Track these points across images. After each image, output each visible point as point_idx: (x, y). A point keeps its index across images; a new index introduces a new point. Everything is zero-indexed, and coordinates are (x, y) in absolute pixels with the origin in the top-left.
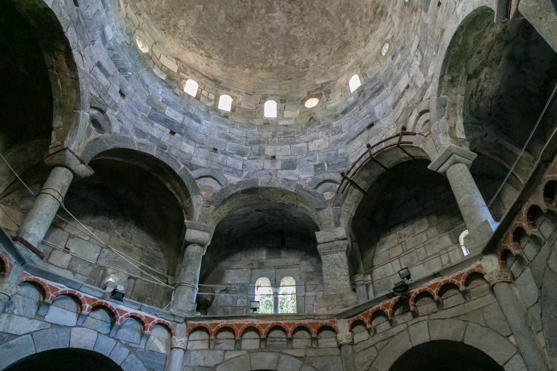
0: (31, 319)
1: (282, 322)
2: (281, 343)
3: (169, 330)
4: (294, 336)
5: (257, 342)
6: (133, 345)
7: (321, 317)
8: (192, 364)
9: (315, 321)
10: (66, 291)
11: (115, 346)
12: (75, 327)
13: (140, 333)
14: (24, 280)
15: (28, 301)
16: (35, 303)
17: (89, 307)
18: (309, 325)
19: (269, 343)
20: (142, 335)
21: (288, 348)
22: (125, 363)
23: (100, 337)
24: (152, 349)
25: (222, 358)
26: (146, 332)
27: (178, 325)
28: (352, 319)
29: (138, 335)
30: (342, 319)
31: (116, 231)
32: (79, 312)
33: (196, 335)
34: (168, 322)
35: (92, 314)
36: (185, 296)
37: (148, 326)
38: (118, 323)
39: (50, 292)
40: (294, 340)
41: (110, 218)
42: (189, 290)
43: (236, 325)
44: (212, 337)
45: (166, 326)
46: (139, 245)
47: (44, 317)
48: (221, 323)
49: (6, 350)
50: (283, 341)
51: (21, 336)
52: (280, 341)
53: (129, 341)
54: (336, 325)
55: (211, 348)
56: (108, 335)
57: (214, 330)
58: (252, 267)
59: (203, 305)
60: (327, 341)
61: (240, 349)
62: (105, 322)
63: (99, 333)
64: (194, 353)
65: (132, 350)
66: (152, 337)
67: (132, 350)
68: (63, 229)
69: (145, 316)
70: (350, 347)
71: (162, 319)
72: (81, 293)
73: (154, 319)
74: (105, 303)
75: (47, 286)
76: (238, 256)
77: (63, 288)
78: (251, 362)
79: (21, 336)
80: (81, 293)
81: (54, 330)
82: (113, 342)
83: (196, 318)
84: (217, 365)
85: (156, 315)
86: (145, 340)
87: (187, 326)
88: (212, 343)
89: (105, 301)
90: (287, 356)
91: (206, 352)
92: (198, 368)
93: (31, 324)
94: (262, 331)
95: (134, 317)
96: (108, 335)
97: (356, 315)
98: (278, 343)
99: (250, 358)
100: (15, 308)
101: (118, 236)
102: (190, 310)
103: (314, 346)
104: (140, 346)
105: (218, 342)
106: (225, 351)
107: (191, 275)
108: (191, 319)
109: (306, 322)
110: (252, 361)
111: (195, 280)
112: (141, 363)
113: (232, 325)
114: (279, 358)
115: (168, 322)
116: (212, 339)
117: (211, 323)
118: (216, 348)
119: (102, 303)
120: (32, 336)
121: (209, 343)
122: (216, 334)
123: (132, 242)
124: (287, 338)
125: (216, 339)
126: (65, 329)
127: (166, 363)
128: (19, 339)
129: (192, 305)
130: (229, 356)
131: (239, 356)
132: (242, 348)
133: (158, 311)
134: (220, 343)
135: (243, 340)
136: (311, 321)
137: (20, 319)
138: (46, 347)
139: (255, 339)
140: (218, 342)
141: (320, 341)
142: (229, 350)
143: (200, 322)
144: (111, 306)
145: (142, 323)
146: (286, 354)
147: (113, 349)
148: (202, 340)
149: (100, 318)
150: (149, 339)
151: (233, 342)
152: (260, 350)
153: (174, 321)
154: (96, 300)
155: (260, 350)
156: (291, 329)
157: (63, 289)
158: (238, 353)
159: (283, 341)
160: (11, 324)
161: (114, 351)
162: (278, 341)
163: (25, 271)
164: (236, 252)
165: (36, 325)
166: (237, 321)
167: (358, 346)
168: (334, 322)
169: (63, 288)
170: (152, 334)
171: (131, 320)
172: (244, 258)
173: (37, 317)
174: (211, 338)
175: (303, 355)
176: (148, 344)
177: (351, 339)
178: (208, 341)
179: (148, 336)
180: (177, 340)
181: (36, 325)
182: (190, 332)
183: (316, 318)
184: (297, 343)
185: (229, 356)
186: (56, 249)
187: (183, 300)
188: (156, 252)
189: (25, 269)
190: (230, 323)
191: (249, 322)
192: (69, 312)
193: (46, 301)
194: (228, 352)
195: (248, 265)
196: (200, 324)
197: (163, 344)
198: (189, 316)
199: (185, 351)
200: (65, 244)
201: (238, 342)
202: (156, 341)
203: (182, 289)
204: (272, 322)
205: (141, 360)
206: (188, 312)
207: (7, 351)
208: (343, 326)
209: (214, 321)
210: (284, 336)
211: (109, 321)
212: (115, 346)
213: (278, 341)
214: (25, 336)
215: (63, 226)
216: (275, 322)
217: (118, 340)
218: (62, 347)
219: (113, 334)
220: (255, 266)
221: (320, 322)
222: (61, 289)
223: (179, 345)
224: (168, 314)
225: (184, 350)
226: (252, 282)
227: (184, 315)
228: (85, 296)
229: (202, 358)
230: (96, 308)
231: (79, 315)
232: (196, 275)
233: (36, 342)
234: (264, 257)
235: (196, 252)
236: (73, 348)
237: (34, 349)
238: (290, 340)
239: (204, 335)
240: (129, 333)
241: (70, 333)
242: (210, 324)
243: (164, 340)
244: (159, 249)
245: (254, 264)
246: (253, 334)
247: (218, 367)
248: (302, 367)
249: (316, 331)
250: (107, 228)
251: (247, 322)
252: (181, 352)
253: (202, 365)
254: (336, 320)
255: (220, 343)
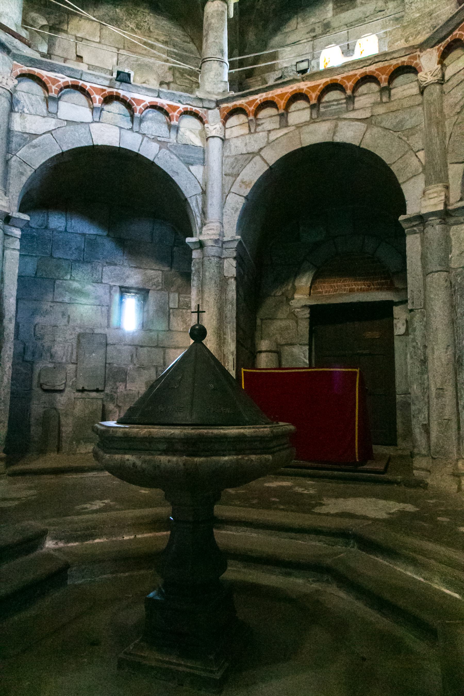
0: (44, 117)
1: (339, 77)
2: (339, 106)
3: (200, 119)
4: (356, 94)
5: (308, 112)
6: (163, 139)
7: (395, 55)
8: (234, 153)
9: (386, 64)
10: (68, 82)
11: (142, 141)
12: (92, 122)
13: (166, 125)
14: (19, 73)
15: (33, 98)
16: (41, 99)
17: (99, 99)
18: (377, 72)
19: (322, 110)
20: (170, 127)
21: (347, 111)
22: (158, 158)
23: (123, 132)
24: (184, 142)
25: (266, 140)
26: (172, 123)
27: (210, 111)
28: (443, 43)
29: (165, 128)
30: (428, 50)
31: (128, 23)
32: (92, 107)
33: (234, 120)
34: (197, 109)
35: (107, 107)
36: (212, 74)
37: (173, 116)
38: (137, 114)
39: (51, 85)
40: (356, 99)
41: (116, 6)
42: (215, 65)
43: (278, 96)
44: (251, 117)
45: (195, 115)
46: (162, 38)
47: (56, 114)
48: (260, 98)
49: (32, 150)
50: (342, 104)
51: (41, 135)
52: (338, 104)
53: (157, 135)
54: (418, 61)
55: (252, 131)
56: (131, 129)
57: (252, 108)
58: (313, 34)
59: (239, 83)
60: (405, 88)
61: (287, 126)
62: (124, 115)
63: (121, 128)
64: (235, 141)
65: (163, 144)
66: (182, 130)
67: (163, 144)
68: (66, 32)
69: (168, 105)
70: (438, 87)
71: (189, 107)
72: (86, 83)
73: (179, 107)
74: (116, 92)
75: (46, 78)
76: (293, 23)
77: (63, 78)
78: (300, 138)
79: (41, 135)
80: (86, 83)
81: (72, 128)
82: (139, 137)
83: (228, 98)
84: (261, 149)
85: (180, 102)
86: (175, 133)
87: (220, 111)
88: (254, 125)
89: (115, 90)
90: (346, 122)
91: (247, 137)
92: (241, 156)
93: (45, 122)
94: (311, 96)
95: (154, 107)
96: (131, 129)
97: (451, 32)
98: (334, 107)
99: (299, 133)
100: (23, 107)
101: (132, 29)
102: (221, 91)
103: (385, 99)
104: (171, 140)
105: (260, 122)
106: (269, 131)
107: (215, 44)
108: (223, 101)
109: (373, 68)
110: (302, 136)
111: (222, 52)
112: (175, 157)
113: (273, 97)
114: (336, 126)
115: (197, 109)
116: (251, 120)
117: (247, 100)
118: (257, 130)
119: (113, 92)
120: (52, 134)
121: (249, 126)
122: (256, 114)
123: (151, 35)
124: (346, 98)
125: (257, 119)
126: (83, 125)
127: (204, 156)
128: (40, 138)
129: (223, 84)
130: (273, 136)
131: (286, 134)
132: (289, 124)
133: (181, 96)
134: (262, 124)
135: (289, 115)
136: (380, 65)
137: (34, 118)
138: (70, 145)
139: (304, 109)
140: (260, 122)
141: (393, 92)
142: (274, 129)
143: (235, 103)
144: (124, 96)
145: (166, 113)
146: (345, 119)
147: (141, 144)
148: (240, 125)
149: (117, 111)
150: (179, 132)
151: (278, 118)
152: (312, 121)
153: (203, 107)
154: (105, 90)
155: (312, 121)
156: (351, 83)
157: (64, 80)
158: (285, 131)
159: (342, 104)
160: (26, 123)
161: (142, 146)
162: (333, 105)
163: (15, 62)
164: (289, 19)
165: (51, 124)
166: (278, 91)
167: (450, 83)
168: (415, 58)
169: (63, 78)
170: (181, 126)
171: (153, 112)
172: (301, 25)
173: (50, 115)
174: (250, 118)
175: (368, 115)
176: (179, 136)
177: (440, 75)
178: (247, 125)
179: (177, 129)
180: (211, 128)
181: (51, 124)
182: (226, 119)
183: (388, 58)
184: (360, 101)
185: (273, 136)
186: (68, 59)
187: (210, 80)
188: (186, 44)
189: (14, 60)
190: (270, 96)
191: (295, 88)
192: (81, 107)
193: (50, 94)
194: (272, 133)
195: (308, 33)
196: (235, 105)
197: (197, 136)
198: (220, 98)
199: (223, 140)
200: (75, 51)
201: (283, 117)
202: (188, 133)
203: (206, 66)
204: (324, 81)
205: (176, 155)
206: (219, 94)
207: (34, 150)
208: (428, 62)
209: (251, 98)
210: (343, 96)
211: (128, 114)
212: (142, 141)
213: (333, 105)
214: (45, 135)
215: (65, 27)
216: (328, 79)
217: (144, 134)
218: (87, 145)
219: (136, 128)
220: (319, 31)
221: (394, 62)
222: (62, 81)
223: (213, 134)
224: (195, 98)
225: (221, 138)
226: (315, 56)
227: (215, 97)
228: (90, 86)
229: (244, 144)
230: (109, 99)
231: (93, 109)
232: (221, 44)
233: (58, 141)
234: (330, 14)
235: (217, 11)
236: (97, 145)
237: (58, 147)
238: (351, 99)
239: (242, 118)
240: (154, 125)
241: (90, 130)
242: (247, 103)
243: (197, 132)
244: (188, 40)
245: (317, 29)
246: (301, 104)
247: (263, 151)
248: (366, 130)
249: (387, 77)
250: (116, 21)
251: (291, 88)
252: (219, 141)
253: (245, 152)
254: (418, 53)
255: (262, 124)
